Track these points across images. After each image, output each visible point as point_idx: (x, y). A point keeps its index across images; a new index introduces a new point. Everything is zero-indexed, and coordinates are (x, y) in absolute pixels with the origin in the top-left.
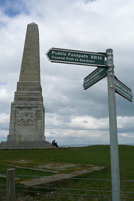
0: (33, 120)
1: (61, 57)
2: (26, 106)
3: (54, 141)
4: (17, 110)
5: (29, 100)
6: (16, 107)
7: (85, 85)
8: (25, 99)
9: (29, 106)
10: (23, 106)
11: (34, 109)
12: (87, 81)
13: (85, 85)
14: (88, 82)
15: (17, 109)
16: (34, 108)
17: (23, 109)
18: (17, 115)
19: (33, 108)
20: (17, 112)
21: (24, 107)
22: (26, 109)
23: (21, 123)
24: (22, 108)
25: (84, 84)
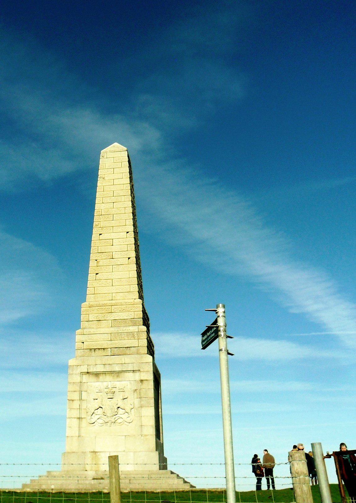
0: (128, 409)
1: (264, 487)
2: (108, 369)
3: (202, 349)
4: (84, 381)
5: (117, 353)
6: (82, 373)
7: (204, 343)
8: (104, 349)
9: (117, 368)
10: (100, 369)
11: (130, 375)
12: (205, 337)
13: (204, 343)
14: (206, 339)
15: (85, 378)
16: (131, 374)
17: (101, 377)
18: (84, 395)
19: (127, 374)
20: (85, 387)
21: (104, 373)
22: (108, 378)
23: (98, 417)
24: (97, 374)
25: (203, 341)
